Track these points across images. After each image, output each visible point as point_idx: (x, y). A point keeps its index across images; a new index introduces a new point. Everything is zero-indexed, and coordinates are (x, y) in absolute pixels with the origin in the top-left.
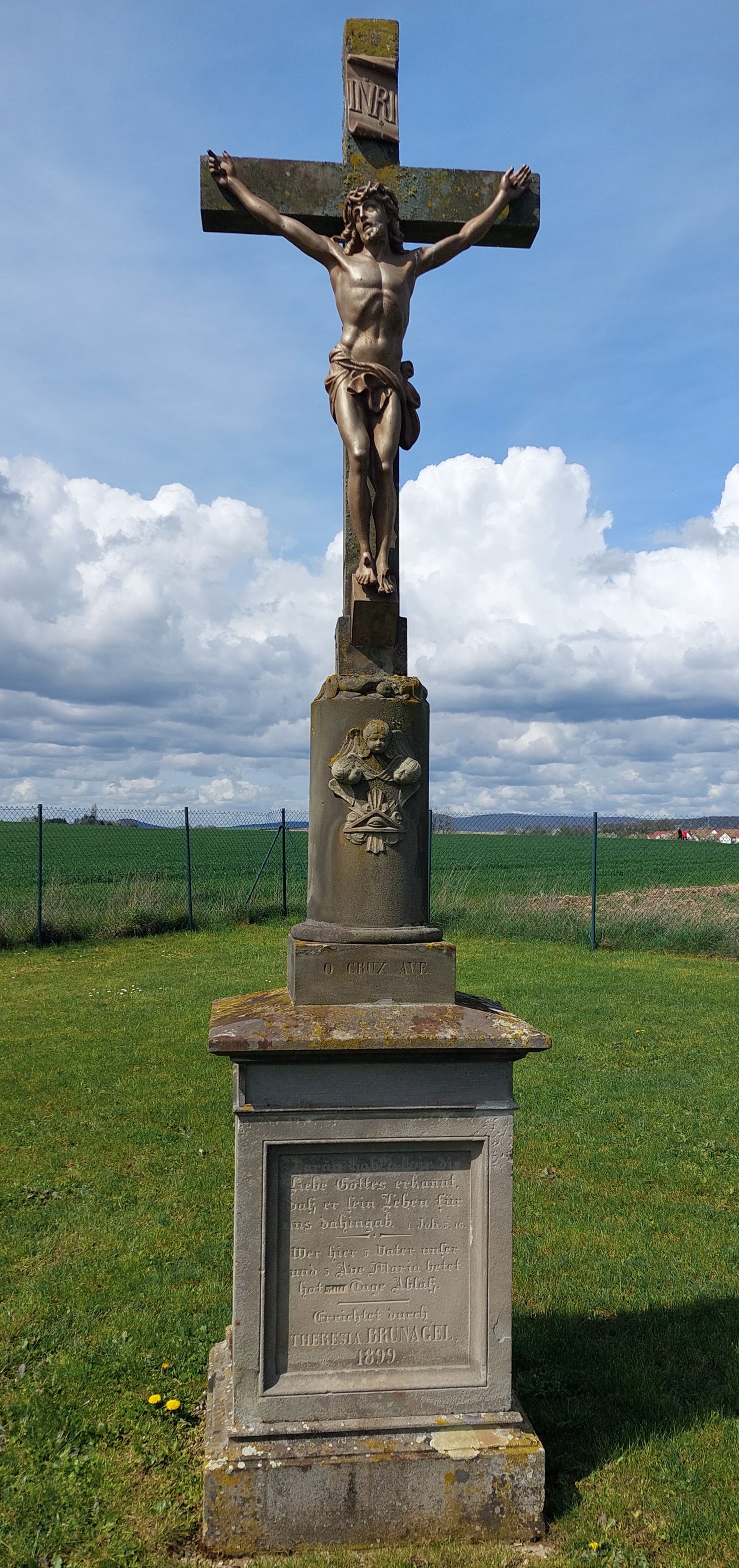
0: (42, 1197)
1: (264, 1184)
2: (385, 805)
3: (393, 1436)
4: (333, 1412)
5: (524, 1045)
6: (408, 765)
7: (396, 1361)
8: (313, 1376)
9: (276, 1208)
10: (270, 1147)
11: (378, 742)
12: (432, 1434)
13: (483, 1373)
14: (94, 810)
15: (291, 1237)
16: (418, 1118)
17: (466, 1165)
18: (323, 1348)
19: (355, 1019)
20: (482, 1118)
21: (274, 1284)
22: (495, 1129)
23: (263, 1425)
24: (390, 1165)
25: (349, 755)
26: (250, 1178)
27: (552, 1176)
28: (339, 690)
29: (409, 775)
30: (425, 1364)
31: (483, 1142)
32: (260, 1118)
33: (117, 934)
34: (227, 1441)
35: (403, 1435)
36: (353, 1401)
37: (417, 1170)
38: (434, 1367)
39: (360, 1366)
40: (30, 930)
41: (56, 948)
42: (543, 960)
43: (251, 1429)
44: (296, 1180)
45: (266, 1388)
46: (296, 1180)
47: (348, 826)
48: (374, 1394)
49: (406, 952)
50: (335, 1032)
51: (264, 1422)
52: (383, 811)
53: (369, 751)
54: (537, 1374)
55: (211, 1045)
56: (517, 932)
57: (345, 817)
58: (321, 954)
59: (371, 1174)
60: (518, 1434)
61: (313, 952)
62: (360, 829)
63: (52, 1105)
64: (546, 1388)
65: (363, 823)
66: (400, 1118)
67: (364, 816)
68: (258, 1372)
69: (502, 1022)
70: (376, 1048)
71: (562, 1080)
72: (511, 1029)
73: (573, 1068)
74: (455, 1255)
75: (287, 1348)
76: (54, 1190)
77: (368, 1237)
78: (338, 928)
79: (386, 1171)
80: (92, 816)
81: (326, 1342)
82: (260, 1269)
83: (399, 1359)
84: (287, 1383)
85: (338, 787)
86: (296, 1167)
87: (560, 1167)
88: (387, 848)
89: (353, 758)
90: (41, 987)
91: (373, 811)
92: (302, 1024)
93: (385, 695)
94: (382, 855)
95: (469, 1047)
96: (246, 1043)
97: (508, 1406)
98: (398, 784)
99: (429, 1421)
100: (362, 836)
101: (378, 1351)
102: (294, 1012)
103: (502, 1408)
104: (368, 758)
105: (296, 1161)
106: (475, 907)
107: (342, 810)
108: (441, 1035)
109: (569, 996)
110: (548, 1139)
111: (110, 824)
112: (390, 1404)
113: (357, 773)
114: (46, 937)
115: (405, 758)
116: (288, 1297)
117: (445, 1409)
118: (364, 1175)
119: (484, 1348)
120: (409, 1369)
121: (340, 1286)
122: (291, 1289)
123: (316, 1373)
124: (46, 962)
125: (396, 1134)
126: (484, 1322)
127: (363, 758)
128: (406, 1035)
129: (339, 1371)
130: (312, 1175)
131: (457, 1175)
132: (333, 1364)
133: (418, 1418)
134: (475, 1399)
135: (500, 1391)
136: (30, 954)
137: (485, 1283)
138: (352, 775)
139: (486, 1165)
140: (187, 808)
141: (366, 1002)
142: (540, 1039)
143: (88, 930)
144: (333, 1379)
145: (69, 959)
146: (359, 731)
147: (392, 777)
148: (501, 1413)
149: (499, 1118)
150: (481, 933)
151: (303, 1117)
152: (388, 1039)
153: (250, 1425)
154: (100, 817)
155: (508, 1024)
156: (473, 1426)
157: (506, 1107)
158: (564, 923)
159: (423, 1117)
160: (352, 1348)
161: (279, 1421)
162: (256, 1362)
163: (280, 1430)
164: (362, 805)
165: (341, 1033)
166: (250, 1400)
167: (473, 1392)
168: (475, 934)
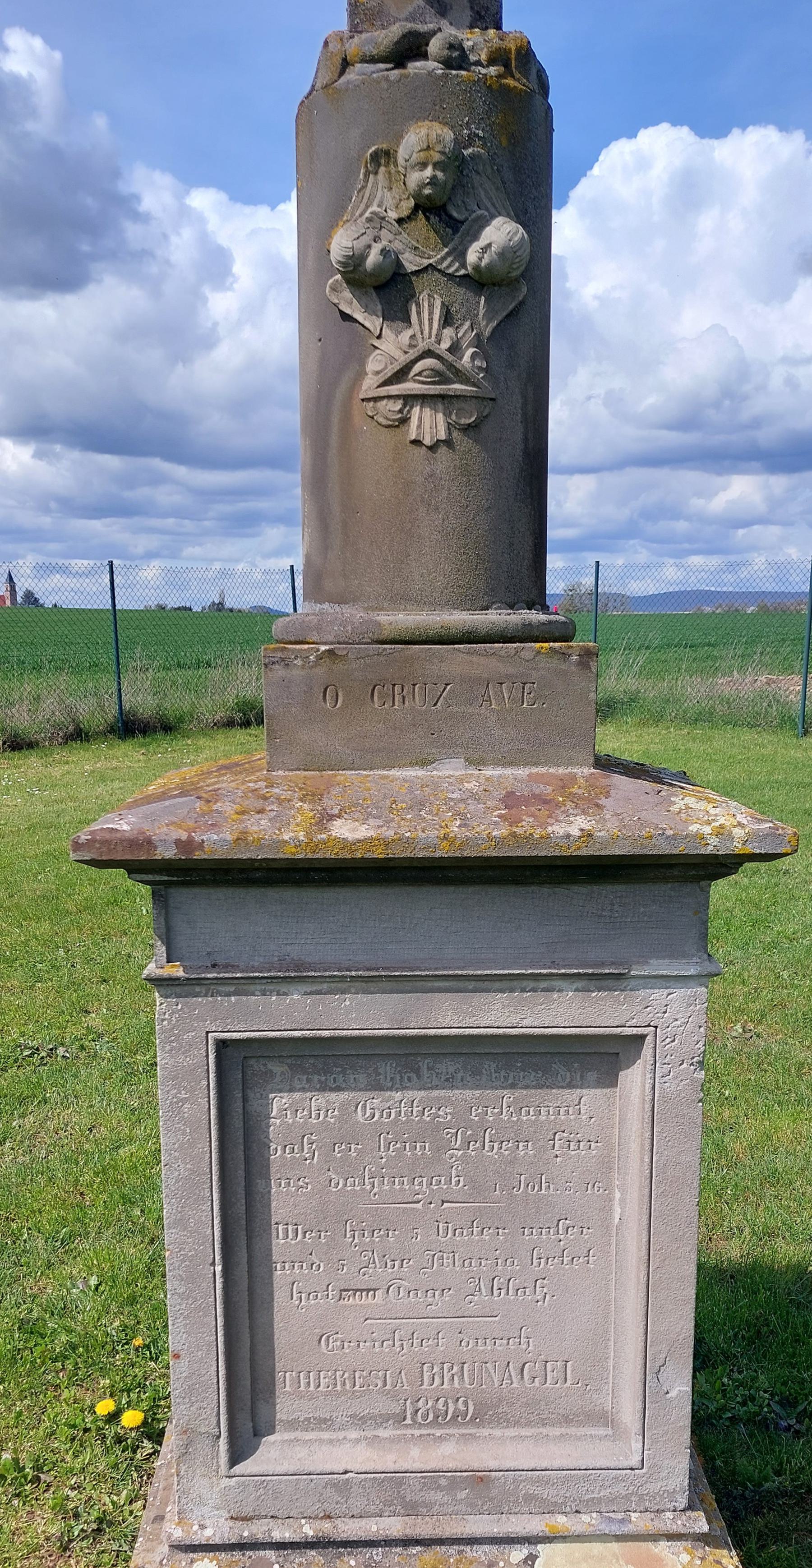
0: (43, 1054)
1: (213, 1112)
2: (448, 332)
3: (467, 1548)
4: (357, 1504)
5: (737, 847)
6: (500, 232)
7: (473, 1419)
8: (321, 1441)
9: (241, 1154)
10: (222, 1045)
11: (429, 172)
12: (540, 1547)
13: (637, 1446)
14: (222, 595)
15: (273, 1204)
16: (512, 991)
17: (610, 1080)
18: (338, 1395)
19: (385, 797)
20: (642, 993)
21: (244, 1284)
22: (669, 1012)
23: (231, 1523)
24: (460, 1075)
25: (367, 214)
26: (184, 1101)
27: (748, 1035)
28: (346, 64)
29: (502, 254)
30: (528, 1424)
31: (643, 1037)
32: (197, 989)
33: (215, 724)
34: (166, 1549)
35: (486, 1548)
36: (393, 1489)
37: (513, 1086)
38: (544, 1431)
39: (407, 1426)
40: (110, 718)
41: (142, 740)
42: (735, 750)
43: (208, 1532)
44: (279, 1102)
45: (235, 1458)
46: (279, 1102)
47: (369, 385)
48: (431, 1477)
49: (493, 662)
50: (338, 823)
51: (232, 1518)
52: (445, 345)
53: (412, 203)
54: (730, 1378)
55: (77, 846)
56: (703, 718)
57: (362, 363)
58: (316, 664)
59: (422, 1093)
60: (700, 1553)
61: (299, 662)
62: (394, 389)
63: (92, 928)
64: (744, 1404)
65: (400, 375)
66: (475, 991)
67: (403, 359)
68: (219, 1437)
69: (691, 801)
70: (421, 855)
71: (761, 901)
72: (708, 818)
73: (776, 885)
74: (586, 1241)
75: (272, 1393)
76: (62, 1045)
77: (419, 1206)
78: (354, 614)
79: (452, 1088)
80: (220, 603)
81: (344, 1384)
82: (213, 1264)
83: (483, 1414)
84: (274, 1453)
85: (347, 294)
86: (277, 1079)
87: (760, 1022)
88: (455, 434)
89: (377, 221)
90: (116, 784)
91: (422, 346)
92: (274, 807)
93: (448, 63)
94: (443, 449)
95: (618, 852)
96: (149, 843)
97: (682, 1501)
98: (479, 282)
99: (534, 1525)
100: (398, 405)
101: (442, 1401)
102: (263, 784)
103: (671, 1506)
104: (409, 218)
105: (277, 1068)
106: (651, 690)
107: (359, 345)
108: (558, 829)
109: (771, 793)
110: (743, 982)
111: (240, 611)
112: (462, 1495)
113: (384, 252)
114: (129, 728)
115: (493, 217)
116: (272, 1307)
117: (565, 1503)
118: (410, 1094)
119: (639, 1405)
120: (498, 1433)
121: (368, 1290)
122: (277, 1295)
123: (326, 1435)
124: (128, 755)
125: (470, 1021)
126: (640, 1361)
127: (400, 221)
128: (485, 830)
129: (369, 1434)
130: (309, 1095)
131: (590, 1098)
132: (360, 1421)
133: (513, 1518)
134: (620, 1489)
135: (668, 1478)
136: (111, 747)
137: (643, 1295)
138: (373, 259)
139: (649, 1081)
140: (292, 567)
141: (411, 765)
142: (772, 834)
143: (181, 720)
144: (359, 1447)
145: (155, 753)
146: (387, 153)
147: (463, 265)
148: (669, 1515)
149: (680, 994)
150: (657, 719)
151: (283, 988)
152: (445, 838)
153: (207, 1522)
154: (228, 605)
155: (703, 805)
156: (616, 1536)
157: (692, 972)
158: (765, 704)
159: (523, 990)
160: (394, 1396)
161: (259, 1517)
162: (214, 1421)
163: (260, 1536)
164: (398, 333)
165: (350, 824)
166: (205, 1482)
167: (616, 1478)
168: (651, 722)
